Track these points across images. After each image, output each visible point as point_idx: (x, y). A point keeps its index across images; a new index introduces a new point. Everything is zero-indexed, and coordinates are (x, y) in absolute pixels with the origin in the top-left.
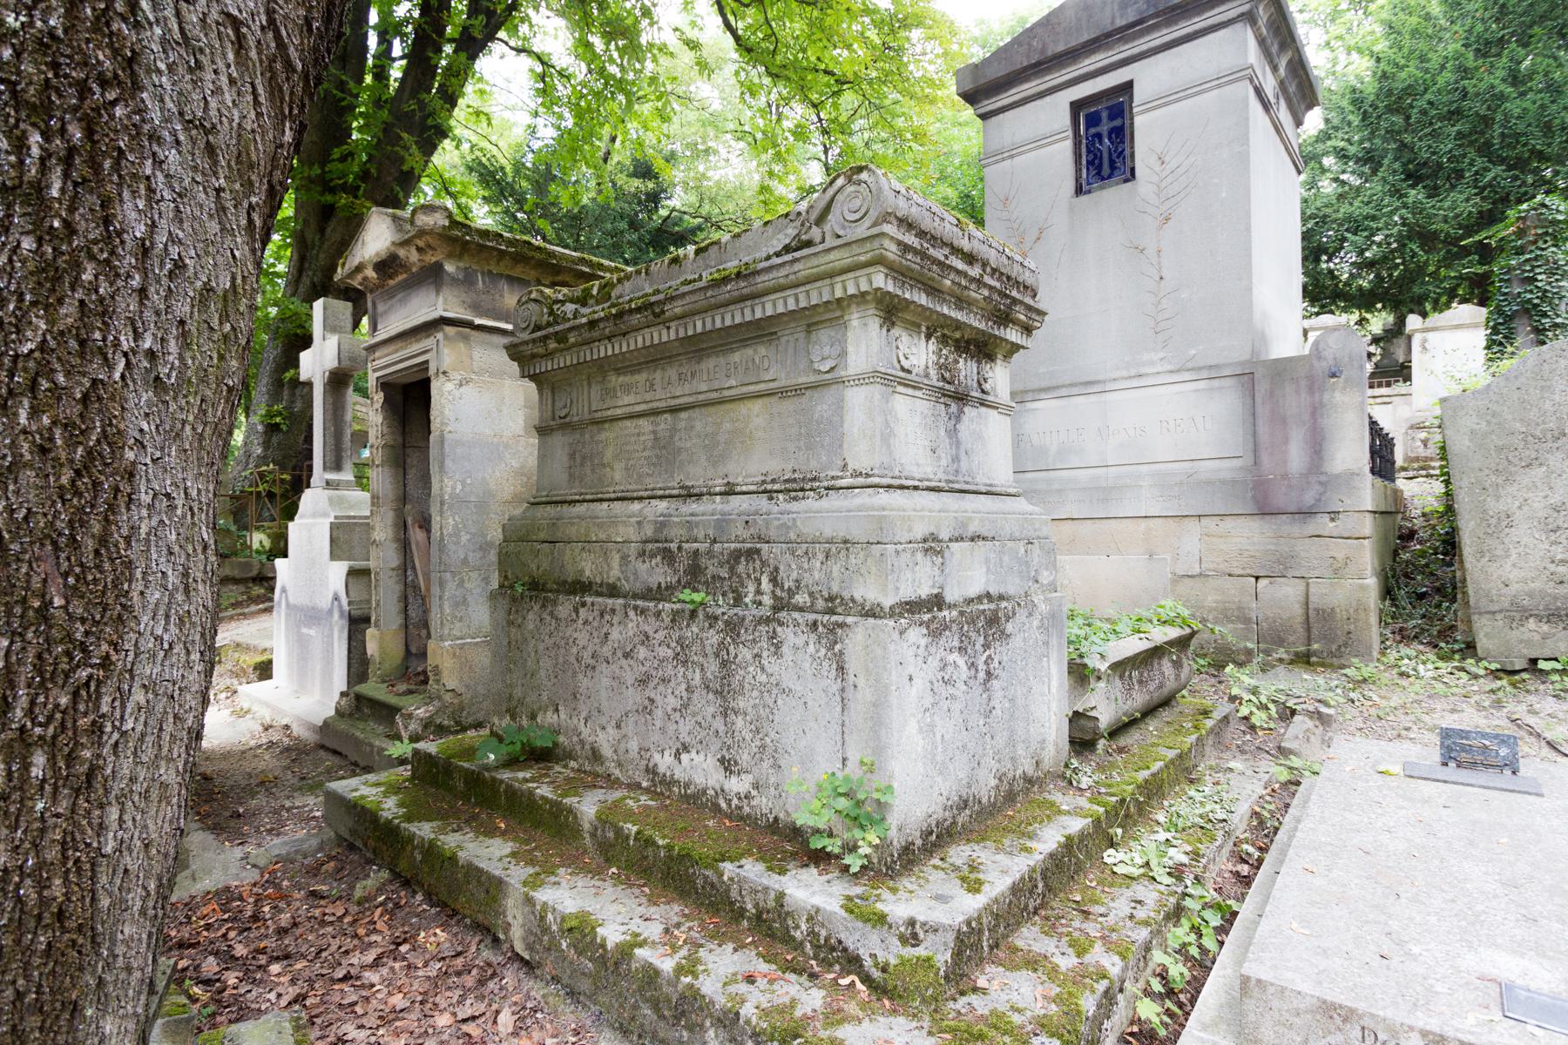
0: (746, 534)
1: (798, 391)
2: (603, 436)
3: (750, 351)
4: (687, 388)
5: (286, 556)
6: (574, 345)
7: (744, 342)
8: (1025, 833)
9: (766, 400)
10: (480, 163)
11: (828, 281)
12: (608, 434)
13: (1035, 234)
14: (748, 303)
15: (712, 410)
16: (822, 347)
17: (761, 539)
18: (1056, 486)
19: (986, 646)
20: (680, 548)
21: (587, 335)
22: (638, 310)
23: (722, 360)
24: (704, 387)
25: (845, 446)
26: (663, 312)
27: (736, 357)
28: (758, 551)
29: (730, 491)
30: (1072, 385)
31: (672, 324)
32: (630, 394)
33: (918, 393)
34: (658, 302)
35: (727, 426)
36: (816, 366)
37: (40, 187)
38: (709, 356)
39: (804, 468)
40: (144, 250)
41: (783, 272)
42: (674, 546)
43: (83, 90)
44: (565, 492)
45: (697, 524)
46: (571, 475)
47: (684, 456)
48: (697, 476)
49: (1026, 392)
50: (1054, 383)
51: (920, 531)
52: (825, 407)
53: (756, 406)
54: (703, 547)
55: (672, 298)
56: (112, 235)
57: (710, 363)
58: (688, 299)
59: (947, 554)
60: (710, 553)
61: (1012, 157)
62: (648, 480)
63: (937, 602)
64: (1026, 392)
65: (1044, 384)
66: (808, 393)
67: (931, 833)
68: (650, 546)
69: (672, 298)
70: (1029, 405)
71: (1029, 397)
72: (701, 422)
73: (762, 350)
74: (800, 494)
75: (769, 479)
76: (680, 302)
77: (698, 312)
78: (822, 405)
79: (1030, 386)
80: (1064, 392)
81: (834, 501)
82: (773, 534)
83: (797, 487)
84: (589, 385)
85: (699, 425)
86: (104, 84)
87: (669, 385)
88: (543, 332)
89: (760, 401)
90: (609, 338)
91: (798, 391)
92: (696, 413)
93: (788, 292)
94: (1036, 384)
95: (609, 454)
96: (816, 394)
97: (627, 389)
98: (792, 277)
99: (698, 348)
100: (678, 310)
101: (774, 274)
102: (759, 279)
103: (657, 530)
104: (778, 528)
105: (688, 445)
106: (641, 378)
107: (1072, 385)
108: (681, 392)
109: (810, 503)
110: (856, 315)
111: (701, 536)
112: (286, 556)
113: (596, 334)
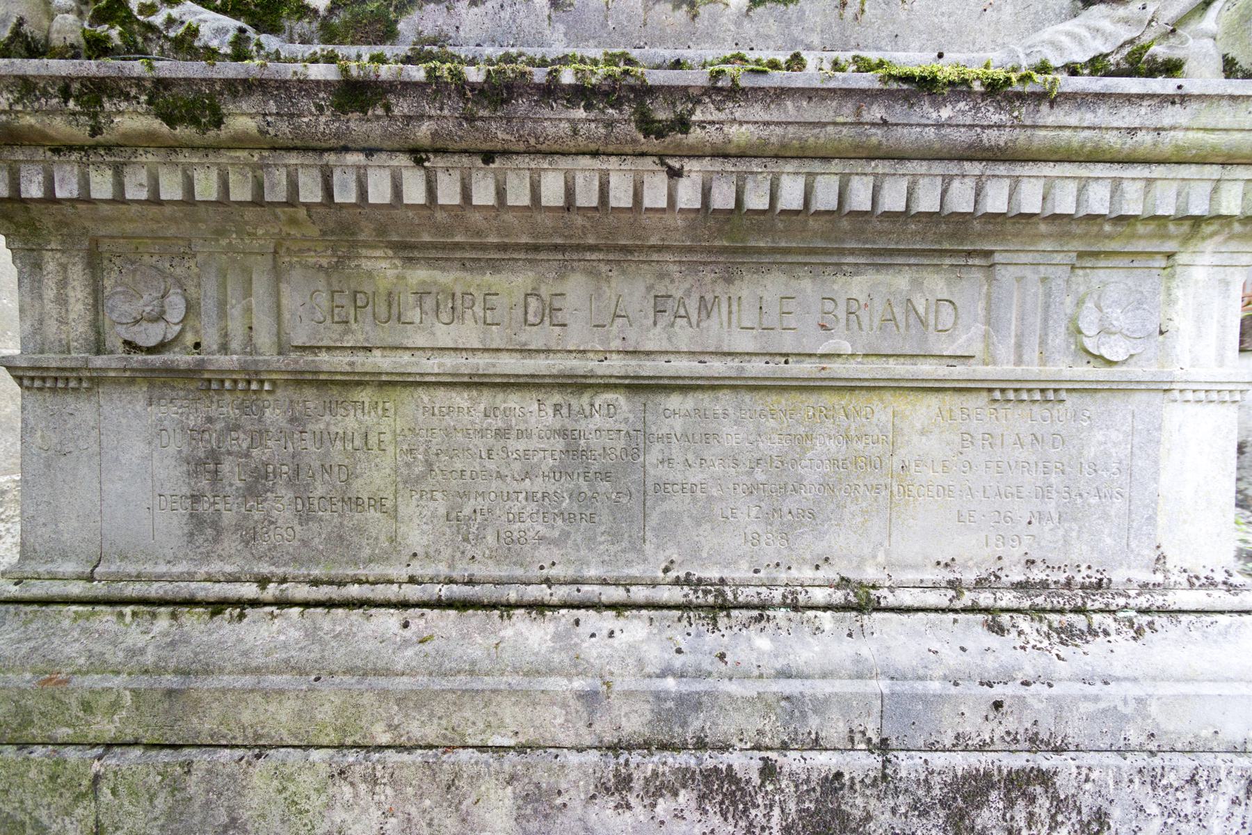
0: (992, 730)
1: (1050, 393)
2: (349, 422)
3: (901, 281)
4: (684, 337)
6: (240, 142)
7: (881, 258)
9: (950, 400)
11: (1214, 172)
12: (355, 418)
14: (975, 168)
15: (773, 399)
16: (1109, 303)
17: (1035, 743)
20: (769, 771)
21: (326, 124)
22: (581, 94)
23: (807, 286)
24: (744, 342)
25: (1161, 520)
26: (683, 124)
27: (858, 286)
28: (1045, 778)
29: (861, 602)
31: (691, 166)
32: (446, 325)
34: (671, 93)
35: (827, 446)
36: (1090, 344)
38: (759, 269)
39: (1054, 558)
41: (1128, 117)
42: (744, 763)
44: (171, 565)
45: (821, 705)
46: (198, 522)
47: (677, 503)
48: (729, 560)
52: (1114, 435)
53: (925, 409)
54: (862, 763)
55: (734, 93)
57: (773, 286)
58: (790, 110)
60: (884, 780)
62: (544, 554)
66: (1071, 401)
68: (644, 765)
69: (734, 93)
72: (738, 427)
73: (937, 284)
74: (1080, 621)
75: (969, 577)
76: (757, 112)
77: (802, 154)
78: (1105, 433)
81: (1169, 648)
82: (1074, 730)
83: (1069, 605)
84: (277, 274)
85: (732, 435)
87: (597, 318)
88: (31, 67)
89: (933, 400)
90: (418, 154)
91: (1050, 393)
92: (726, 399)
93: (1099, 170)
95: (375, 476)
96: (1093, 406)
97: (452, 306)
98: (1146, 138)
99: (734, 242)
100: (739, 134)
101: (1102, 116)
102: (1048, 116)
103: (661, 717)
104: (1091, 718)
105: (695, 476)
106: (512, 283)
108: (673, 346)
109: (1114, 652)
110: (1207, 259)
111: (835, 730)
113: (356, 125)
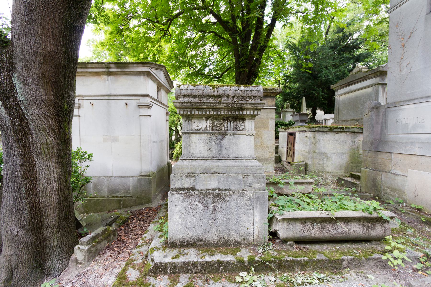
5: (325, 114)
8: (213, 255)
10: (289, 45)
13: (409, 35)
18: (411, 141)
19: (213, 202)
30: (421, 98)
33: (203, 135)
37: (22, 138)
40: (32, 142)
43: (23, 128)
49: (401, 102)
50: (413, 97)
51: (186, 171)
56: (29, 141)
59: (197, 177)
61: (401, 5)
63: (193, 189)
64: (401, 102)
65: (409, 98)
67: (201, 240)
70: (402, 107)
71: (402, 104)
79: (403, 99)
80: (417, 101)
86: (25, 127)
94: (406, 98)
107: (421, 98)
112: (325, 114)
